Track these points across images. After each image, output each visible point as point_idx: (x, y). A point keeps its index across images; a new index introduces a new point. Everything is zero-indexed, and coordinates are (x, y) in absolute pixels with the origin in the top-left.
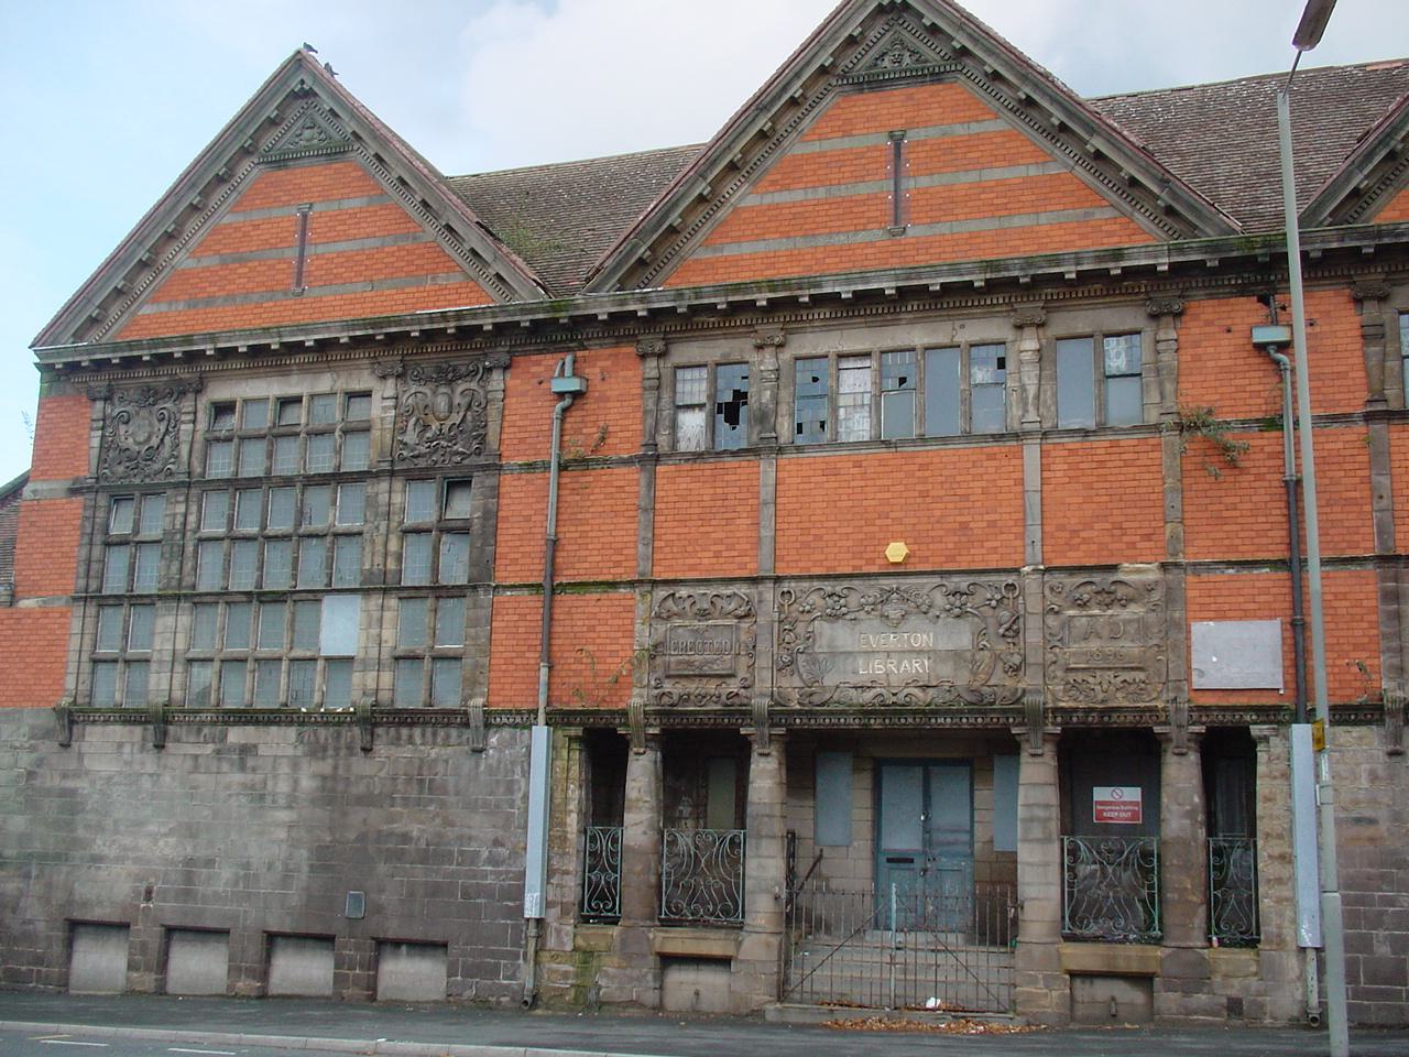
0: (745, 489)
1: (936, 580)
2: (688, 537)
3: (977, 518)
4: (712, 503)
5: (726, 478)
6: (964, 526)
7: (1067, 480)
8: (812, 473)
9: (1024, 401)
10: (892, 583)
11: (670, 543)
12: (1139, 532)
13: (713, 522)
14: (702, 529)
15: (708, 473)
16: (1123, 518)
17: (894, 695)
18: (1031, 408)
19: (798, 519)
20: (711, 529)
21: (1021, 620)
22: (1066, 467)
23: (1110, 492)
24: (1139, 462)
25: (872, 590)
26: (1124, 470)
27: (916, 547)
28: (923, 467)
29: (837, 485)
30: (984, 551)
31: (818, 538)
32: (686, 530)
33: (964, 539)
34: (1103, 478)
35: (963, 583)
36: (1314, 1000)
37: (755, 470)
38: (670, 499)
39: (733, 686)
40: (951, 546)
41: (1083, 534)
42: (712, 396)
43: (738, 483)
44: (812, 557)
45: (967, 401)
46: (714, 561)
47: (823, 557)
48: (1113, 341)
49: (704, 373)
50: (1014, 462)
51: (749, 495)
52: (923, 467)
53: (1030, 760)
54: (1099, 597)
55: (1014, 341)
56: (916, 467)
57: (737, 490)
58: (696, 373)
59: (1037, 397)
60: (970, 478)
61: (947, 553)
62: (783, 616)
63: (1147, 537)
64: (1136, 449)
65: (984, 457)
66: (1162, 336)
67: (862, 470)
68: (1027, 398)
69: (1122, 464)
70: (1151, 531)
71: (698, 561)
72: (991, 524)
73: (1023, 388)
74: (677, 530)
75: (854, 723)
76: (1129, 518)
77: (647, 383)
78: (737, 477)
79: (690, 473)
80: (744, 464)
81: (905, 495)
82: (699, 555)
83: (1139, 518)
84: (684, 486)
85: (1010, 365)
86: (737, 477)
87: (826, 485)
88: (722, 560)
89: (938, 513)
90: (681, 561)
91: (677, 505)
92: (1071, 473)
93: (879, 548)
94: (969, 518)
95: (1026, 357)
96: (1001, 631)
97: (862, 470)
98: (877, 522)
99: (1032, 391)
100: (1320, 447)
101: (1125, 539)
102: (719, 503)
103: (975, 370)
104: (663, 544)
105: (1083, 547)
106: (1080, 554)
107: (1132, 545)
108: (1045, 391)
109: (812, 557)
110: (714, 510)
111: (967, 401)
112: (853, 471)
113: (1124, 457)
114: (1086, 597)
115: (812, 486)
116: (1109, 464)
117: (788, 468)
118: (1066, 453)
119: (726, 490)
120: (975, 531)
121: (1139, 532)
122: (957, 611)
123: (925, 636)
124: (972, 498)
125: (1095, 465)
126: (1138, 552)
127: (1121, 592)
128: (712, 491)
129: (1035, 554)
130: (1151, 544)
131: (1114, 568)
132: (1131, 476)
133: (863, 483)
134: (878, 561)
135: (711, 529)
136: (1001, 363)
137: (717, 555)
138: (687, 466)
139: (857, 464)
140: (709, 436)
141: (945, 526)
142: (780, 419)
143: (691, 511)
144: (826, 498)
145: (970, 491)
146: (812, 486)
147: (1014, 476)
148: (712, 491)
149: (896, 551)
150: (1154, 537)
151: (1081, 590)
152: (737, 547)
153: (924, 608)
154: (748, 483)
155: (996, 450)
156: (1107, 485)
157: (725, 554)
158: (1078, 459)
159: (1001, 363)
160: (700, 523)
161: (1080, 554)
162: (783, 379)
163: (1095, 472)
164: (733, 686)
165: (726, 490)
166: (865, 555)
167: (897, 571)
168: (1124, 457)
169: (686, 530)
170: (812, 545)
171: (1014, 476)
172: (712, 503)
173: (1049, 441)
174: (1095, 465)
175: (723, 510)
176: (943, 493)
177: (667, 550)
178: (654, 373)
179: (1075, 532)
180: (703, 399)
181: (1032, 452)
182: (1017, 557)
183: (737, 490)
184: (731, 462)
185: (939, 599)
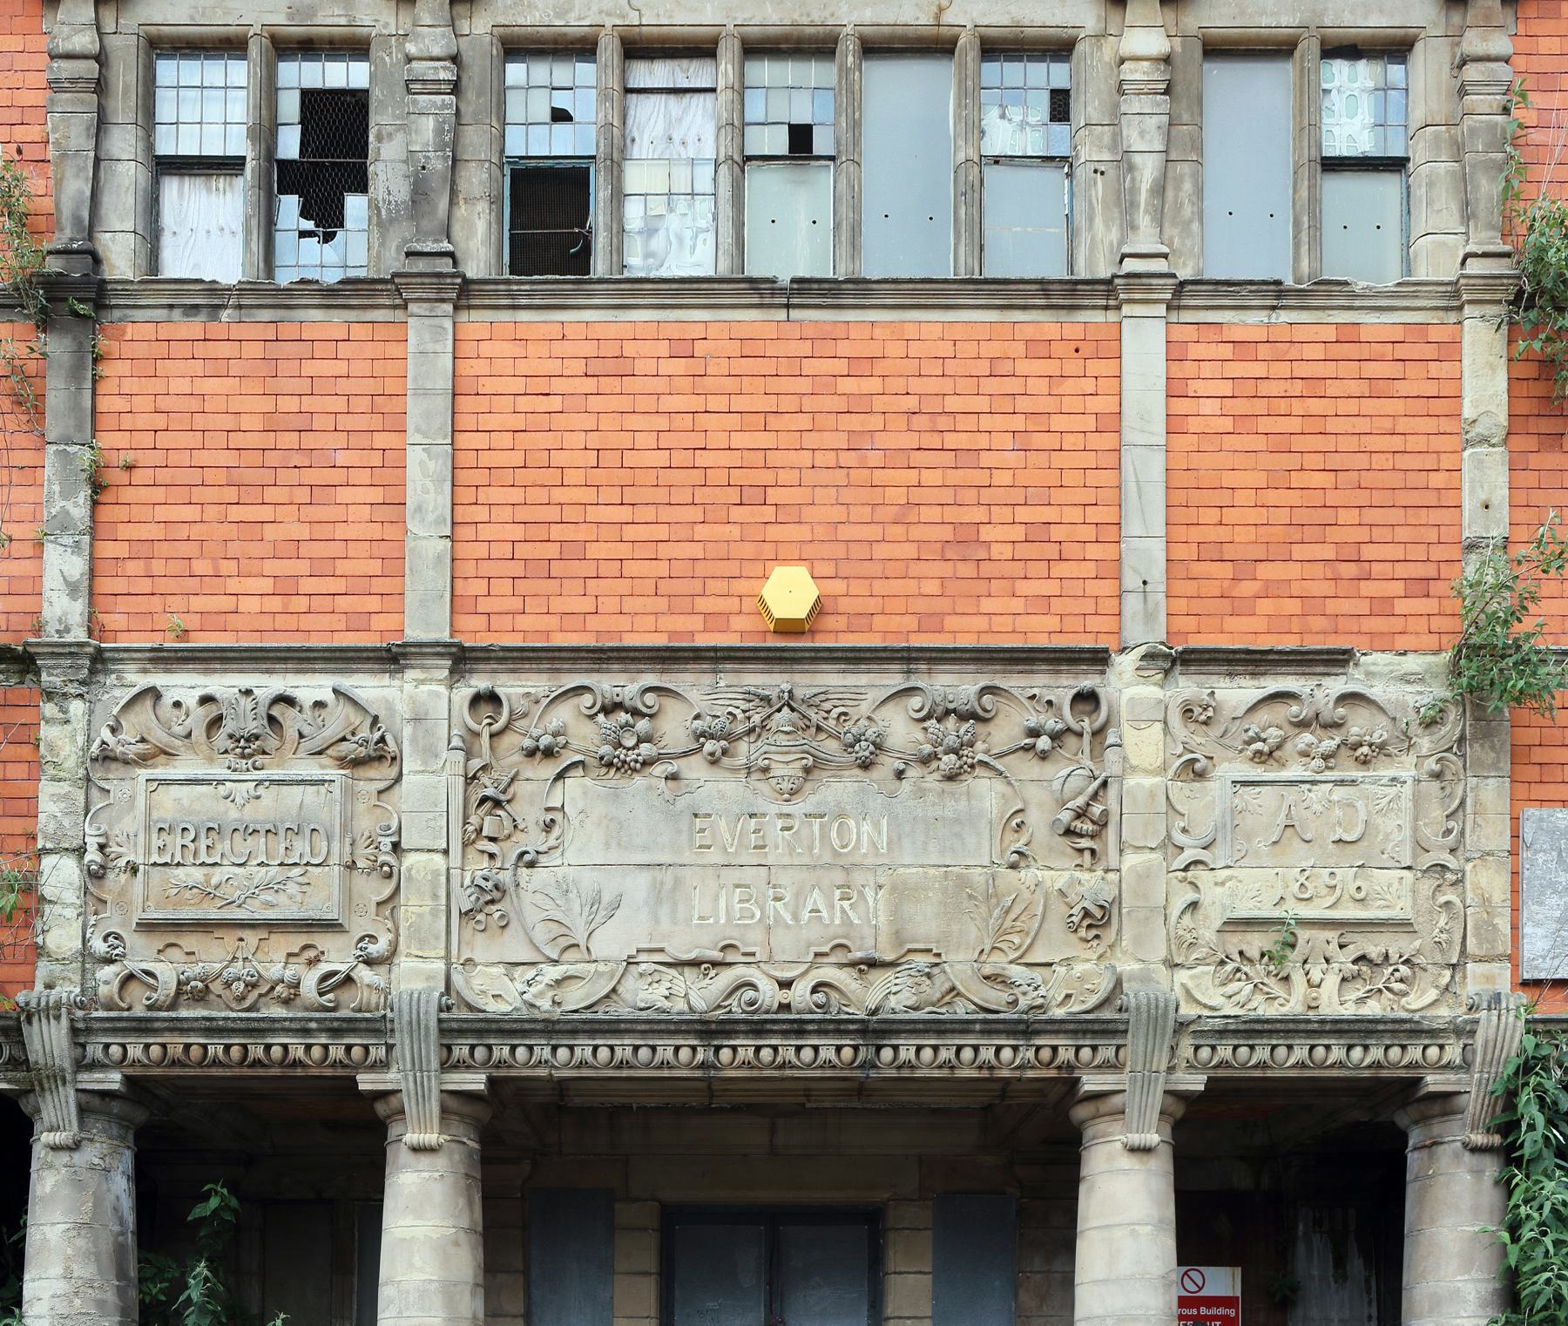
0: (363, 404)
1: (894, 680)
2: (197, 531)
3: (1000, 514)
4: (268, 440)
5: (309, 368)
6: (966, 540)
7: (1227, 424)
8: (554, 367)
9: (1124, 204)
10: (773, 682)
11: (144, 550)
12: (1402, 570)
13: (271, 494)
14: (236, 513)
15: (256, 350)
16: (1362, 534)
17: (786, 985)
18: (1144, 220)
19: (589, 422)
20: (265, 513)
21: (1112, 791)
22: (1226, 388)
23: (1334, 462)
24: (1403, 388)
25: (701, 695)
26: (1369, 406)
27: (838, 587)
28: (861, 365)
29: (624, 403)
30: (1018, 605)
31: (573, 551)
32: (190, 513)
33: (966, 570)
34: (1317, 425)
35: (961, 686)
36: (114, 302)
37: (394, 350)
38: (142, 421)
39: (338, 955)
40: (932, 587)
41: (1264, 571)
42: (265, 130)
43: (344, 386)
44: (557, 605)
45: (972, 195)
46: (275, 604)
47: (587, 605)
48: (1340, 73)
49: (238, 72)
50: (1095, 367)
51: (375, 422)
52: (861, 365)
53: (1127, 1162)
54: (1307, 737)
55: (1101, 36)
56: (841, 366)
57: (339, 404)
58: (214, 71)
59: (1159, 189)
60: (982, 404)
61: (921, 605)
62: (476, 764)
63: (1421, 586)
64: (1402, 351)
65: (1020, 348)
66: (1474, 43)
67: (696, 366)
68: (1134, 190)
69: (1364, 388)
70: (1429, 570)
71: (226, 603)
72: (1037, 533)
73: (1125, 161)
74: (162, 513)
75: (681, 1057)
76: (1377, 534)
77: (67, 68)
78: (340, 368)
79: (200, 349)
80: (359, 332)
81: (810, 440)
82: (233, 585)
83: (1402, 534)
84: (183, 386)
85: (1085, 108)
86: (340, 368)
87: (595, 403)
88: (301, 603)
89: (898, 496)
90: (176, 603)
91: (164, 440)
92: (1240, 406)
93: (741, 586)
94: (979, 514)
95: (1135, 73)
96: (1066, 816)
97: (696, 366)
98: (737, 513)
99: (1148, 169)
100: (391, 603)
101: (1367, 588)
102: (290, 440)
103: (991, 117)
104: (121, 550)
105: (1265, 606)
106: (1258, 624)
107: (1382, 607)
108: (1179, 180)
109: (557, 605)
110: (273, 458)
111: (972, 195)
112: (669, 367)
113: (1372, 369)
114: (1273, 734)
115: (555, 403)
116: (1333, 388)
117: (486, 349)
118: (1227, 351)
119: (308, 403)
120: (996, 550)
121: (1402, 570)
122: (949, 761)
123: (866, 827)
124: (987, 459)
125: (1297, 388)
126: (1398, 624)
127: (1360, 724)
128: (267, 404)
129: (1144, 626)
130: (1430, 605)
131: (1338, 660)
132: (1387, 424)
133: (697, 403)
134: (738, 623)
135: (265, 513)
136: (1060, 106)
137: (285, 589)
138: (193, 327)
139: (683, 349)
140: (257, 246)
141: (917, 532)
142: (462, 211)
143: (203, 458)
144: (594, 440)
145: (983, 441)
146: (555, 403)
147: (1095, 404)
148: (267, 404)
149: (789, 592)
150: (1435, 588)
151: (1264, 716)
152: (342, 567)
153: (864, 749)
154: (370, 386)
155: (1052, 331)
156: (1327, 443)
157: (308, 585)
158: (1258, 369)
159: (1060, 106)
160: (231, 494)
161: (1258, 624)
162: (470, 94)
163: (1298, 407)
164: (338, 955)
165: (308, 403)
166: (703, 604)
167: (790, 646)
168: (1372, 369)
169: (190, 513)
170: (557, 568)
171: (1095, 404)
172: (268, 440)
173: (1187, 316)
174: (1297, 388)
175: (297, 459)
176: (911, 441)
177: (133, 567)
178: (85, 41)
179: (1245, 566)
180: (238, 144)
181: (1144, 338)
182: (1105, 624)
183: (339, 404)
184: (319, 321)
185: (900, 729)
